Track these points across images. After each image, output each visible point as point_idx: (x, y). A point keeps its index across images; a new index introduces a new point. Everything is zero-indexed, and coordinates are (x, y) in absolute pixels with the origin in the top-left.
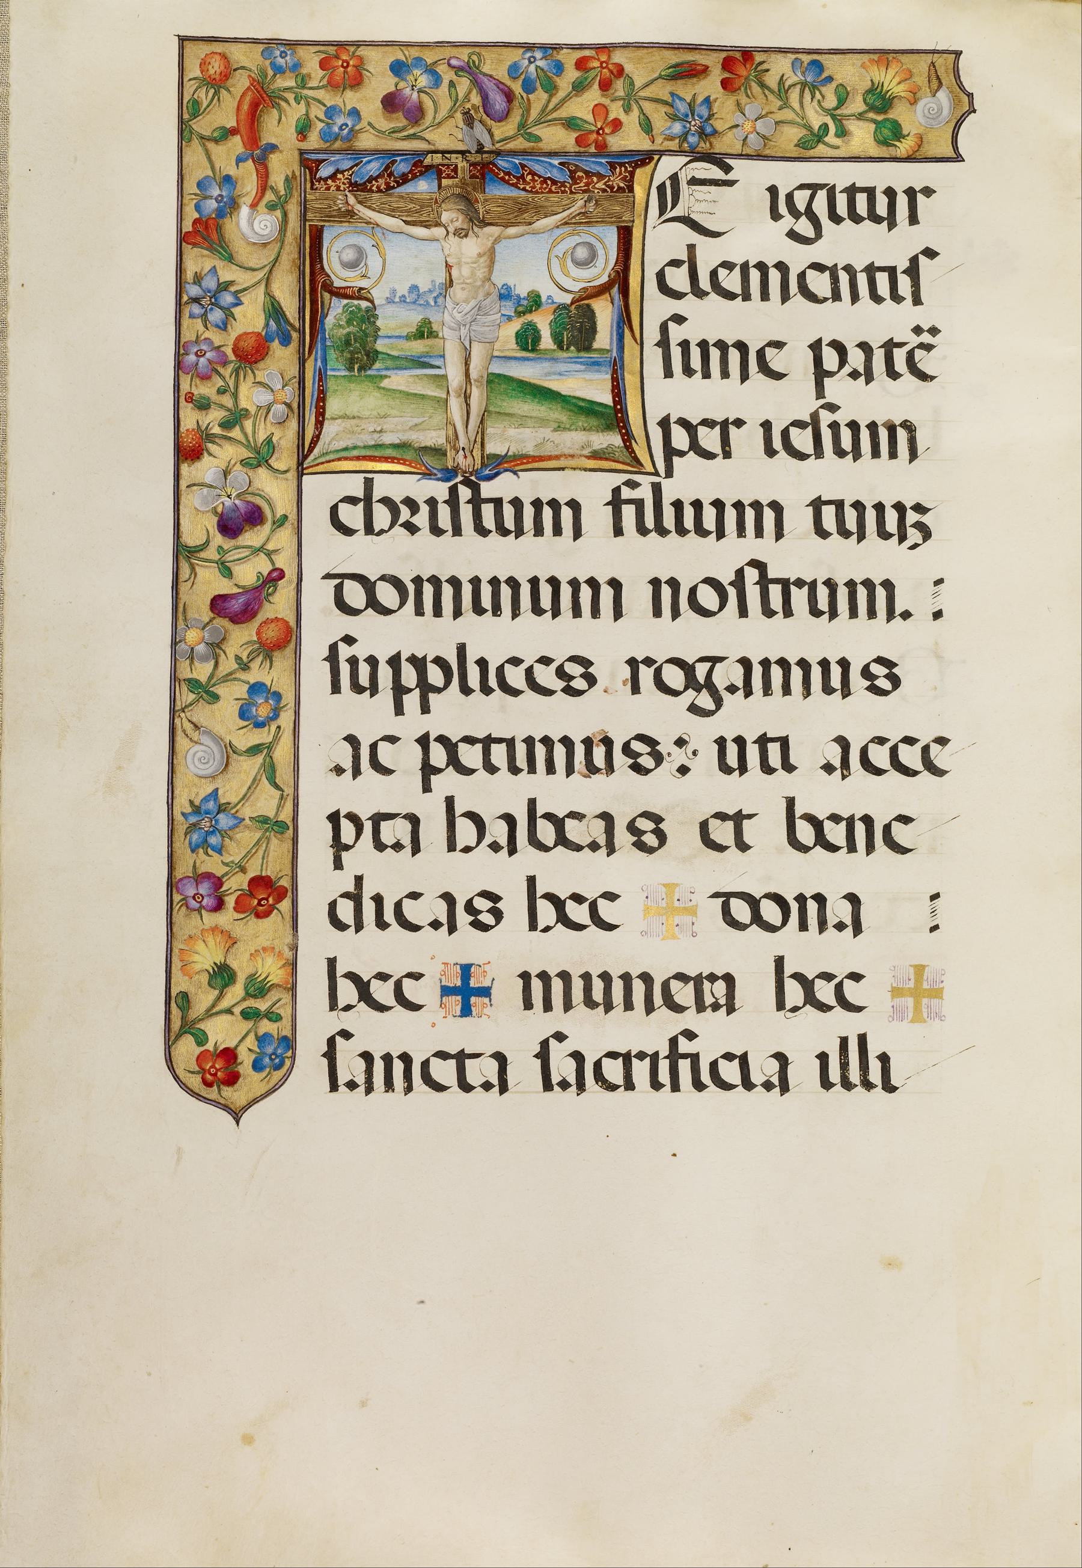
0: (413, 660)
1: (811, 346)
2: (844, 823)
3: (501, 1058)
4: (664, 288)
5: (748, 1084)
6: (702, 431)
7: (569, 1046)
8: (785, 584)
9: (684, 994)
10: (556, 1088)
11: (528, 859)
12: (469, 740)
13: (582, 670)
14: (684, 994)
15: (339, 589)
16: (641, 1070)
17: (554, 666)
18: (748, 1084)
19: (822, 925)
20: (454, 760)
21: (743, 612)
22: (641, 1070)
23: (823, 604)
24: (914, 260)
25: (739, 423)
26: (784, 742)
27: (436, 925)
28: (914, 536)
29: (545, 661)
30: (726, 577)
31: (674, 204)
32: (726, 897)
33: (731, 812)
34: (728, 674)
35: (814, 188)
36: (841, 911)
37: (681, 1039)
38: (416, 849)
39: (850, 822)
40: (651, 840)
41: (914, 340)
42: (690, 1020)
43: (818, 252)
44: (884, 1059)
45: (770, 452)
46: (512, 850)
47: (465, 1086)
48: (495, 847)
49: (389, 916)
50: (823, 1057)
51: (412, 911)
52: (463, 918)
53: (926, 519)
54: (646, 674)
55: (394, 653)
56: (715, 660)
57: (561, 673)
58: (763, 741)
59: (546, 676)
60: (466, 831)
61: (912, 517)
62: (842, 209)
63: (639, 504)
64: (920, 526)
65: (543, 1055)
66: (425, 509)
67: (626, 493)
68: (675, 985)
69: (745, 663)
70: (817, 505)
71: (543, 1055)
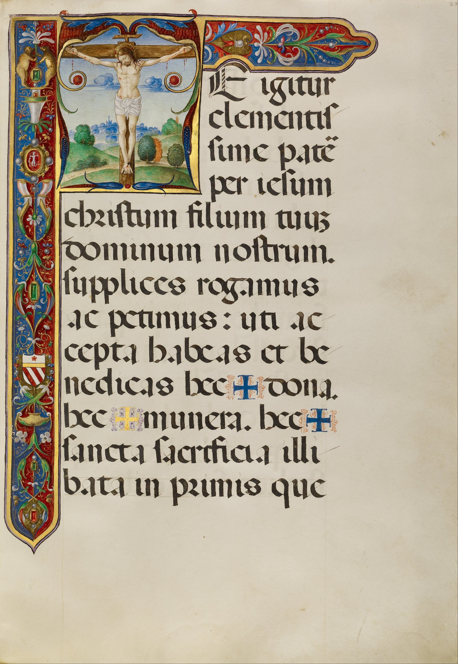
0: (101, 279)
1: (279, 148)
3: (141, 448)
4: (212, 123)
5: (249, 460)
6: (228, 182)
7: (77, 442)
8: (275, 248)
9: (216, 422)
10: (163, 461)
11: (186, 365)
12: (132, 313)
13: (180, 284)
14: (216, 422)
16: (200, 454)
17: (167, 282)
18: (249, 460)
19: (315, 394)
20: (124, 322)
21: (257, 259)
22: (200, 454)
23: (292, 255)
24: (328, 109)
25: (245, 180)
26: (273, 316)
27: (143, 392)
28: (322, 226)
29: (164, 279)
30: (251, 244)
31: (217, 87)
32: (272, 381)
33: (276, 346)
34: (240, 287)
35: (284, 79)
36: (322, 387)
37: (217, 440)
40: (243, 357)
41: (326, 143)
42: (219, 432)
43: (287, 107)
44: (314, 449)
45: (261, 191)
46: (179, 362)
47: (123, 459)
48: (171, 360)
49: (123, 388)
50: (286, 449)
51: (134, 386)
52: (155, 390)
53: (327, 219)
54: (205, 286)
55: (93, 276)
56: (235, 280)
57: (171, 285)
59: (163, 286)
60: (158, 353)
61: (321, 218)
62: (295, 88)
63: (200, 212)
64: (324, 221)
65: (157, 447)
66: (106, 215)
67: (195, 207)
68: (212, 418)
69: (250, 281)
70: (280, 214)
71: (157, 447)
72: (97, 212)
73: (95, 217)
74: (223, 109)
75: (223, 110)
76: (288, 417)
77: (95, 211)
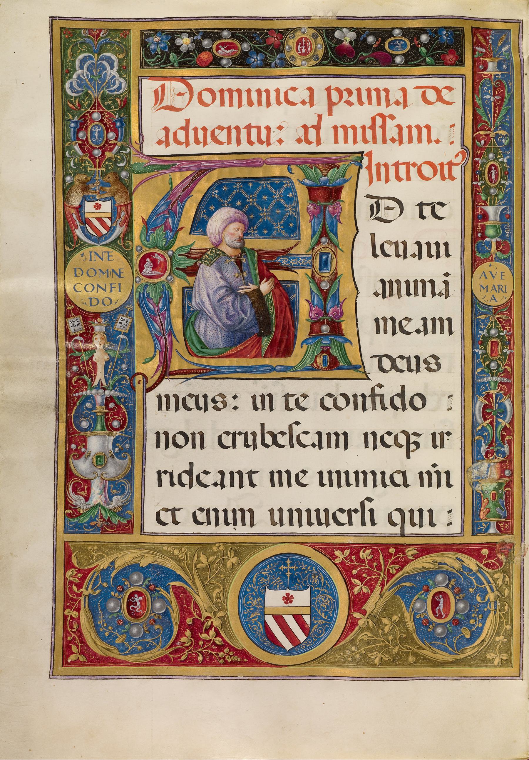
2: (231, 435)
7: (396, 122)
15: (424, 93)
38: (405, 106)
39: (208, 511)
58: (249, 127)
66: (355, 93)
72: (350, 127)
73: (343, 96)
74: (287, 430)
75: (287, 431)
76: (392, 436)
77: (342, 89)
